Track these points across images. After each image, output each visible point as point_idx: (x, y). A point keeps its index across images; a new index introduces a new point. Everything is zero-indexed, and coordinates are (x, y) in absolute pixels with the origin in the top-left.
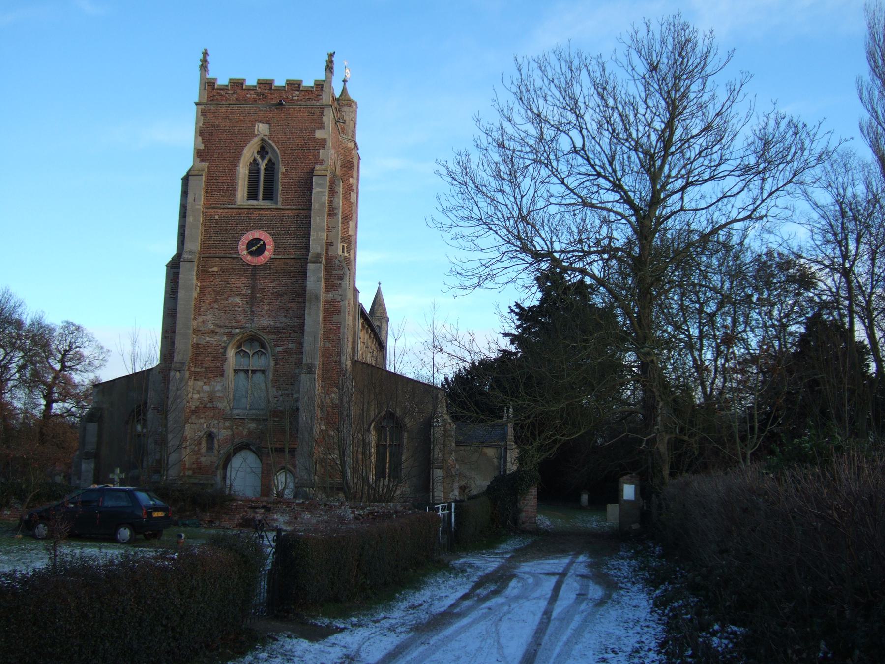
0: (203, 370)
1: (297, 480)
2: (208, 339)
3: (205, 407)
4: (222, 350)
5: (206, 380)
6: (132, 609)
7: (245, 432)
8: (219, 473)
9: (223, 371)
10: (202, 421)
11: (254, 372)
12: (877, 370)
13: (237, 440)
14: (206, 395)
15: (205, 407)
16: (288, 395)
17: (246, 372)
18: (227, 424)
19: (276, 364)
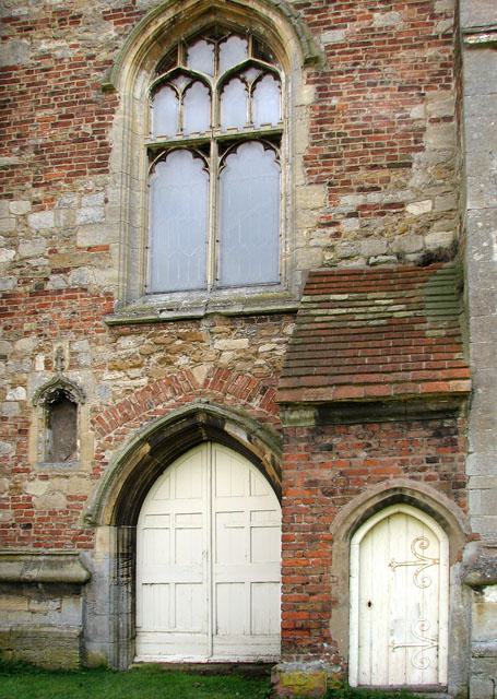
0: (29, 156)
1: (470, 551)
2: (44, 46)
3: (39, 291)
4: (99, 77)
5: (39, 194)
6: (115, 182)
7: (201, 374)
8: (105, 539)
9: (105, 148)
10: (26, 344)
11: (229, 145)
12: (226, 433)
13: (169, 407)
14: (42, 246)
15: (39, 291)
16: (383, 210)
17: (199, 149)
18: (129, 344)
19: (323, 93)
